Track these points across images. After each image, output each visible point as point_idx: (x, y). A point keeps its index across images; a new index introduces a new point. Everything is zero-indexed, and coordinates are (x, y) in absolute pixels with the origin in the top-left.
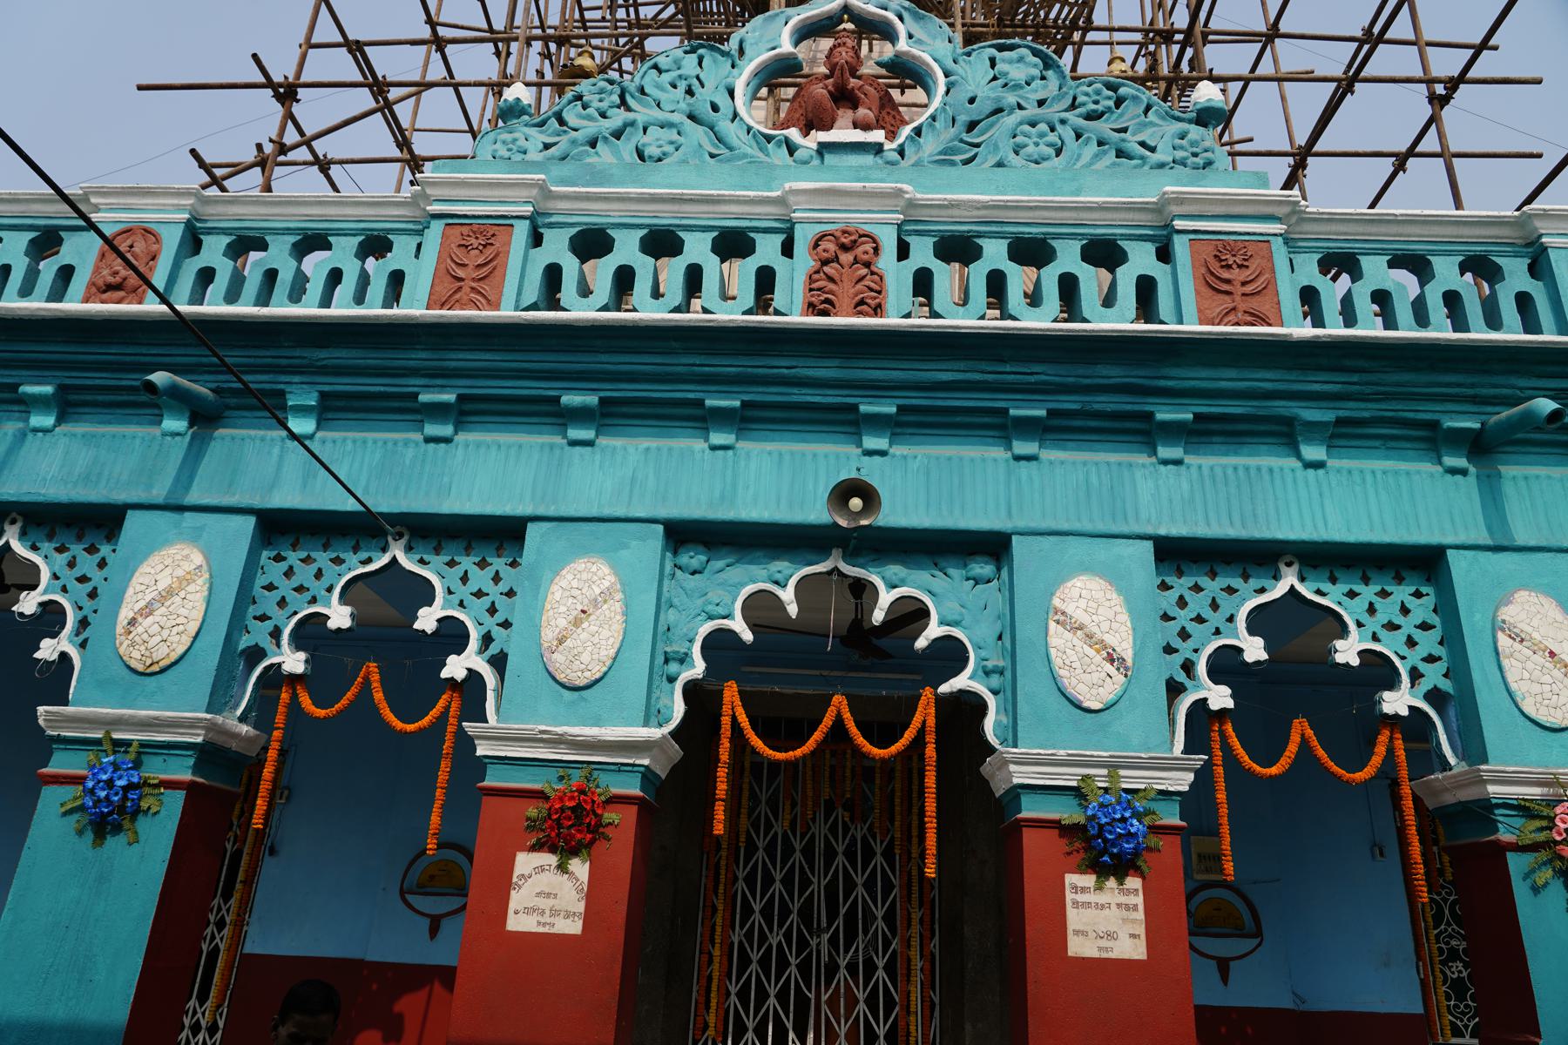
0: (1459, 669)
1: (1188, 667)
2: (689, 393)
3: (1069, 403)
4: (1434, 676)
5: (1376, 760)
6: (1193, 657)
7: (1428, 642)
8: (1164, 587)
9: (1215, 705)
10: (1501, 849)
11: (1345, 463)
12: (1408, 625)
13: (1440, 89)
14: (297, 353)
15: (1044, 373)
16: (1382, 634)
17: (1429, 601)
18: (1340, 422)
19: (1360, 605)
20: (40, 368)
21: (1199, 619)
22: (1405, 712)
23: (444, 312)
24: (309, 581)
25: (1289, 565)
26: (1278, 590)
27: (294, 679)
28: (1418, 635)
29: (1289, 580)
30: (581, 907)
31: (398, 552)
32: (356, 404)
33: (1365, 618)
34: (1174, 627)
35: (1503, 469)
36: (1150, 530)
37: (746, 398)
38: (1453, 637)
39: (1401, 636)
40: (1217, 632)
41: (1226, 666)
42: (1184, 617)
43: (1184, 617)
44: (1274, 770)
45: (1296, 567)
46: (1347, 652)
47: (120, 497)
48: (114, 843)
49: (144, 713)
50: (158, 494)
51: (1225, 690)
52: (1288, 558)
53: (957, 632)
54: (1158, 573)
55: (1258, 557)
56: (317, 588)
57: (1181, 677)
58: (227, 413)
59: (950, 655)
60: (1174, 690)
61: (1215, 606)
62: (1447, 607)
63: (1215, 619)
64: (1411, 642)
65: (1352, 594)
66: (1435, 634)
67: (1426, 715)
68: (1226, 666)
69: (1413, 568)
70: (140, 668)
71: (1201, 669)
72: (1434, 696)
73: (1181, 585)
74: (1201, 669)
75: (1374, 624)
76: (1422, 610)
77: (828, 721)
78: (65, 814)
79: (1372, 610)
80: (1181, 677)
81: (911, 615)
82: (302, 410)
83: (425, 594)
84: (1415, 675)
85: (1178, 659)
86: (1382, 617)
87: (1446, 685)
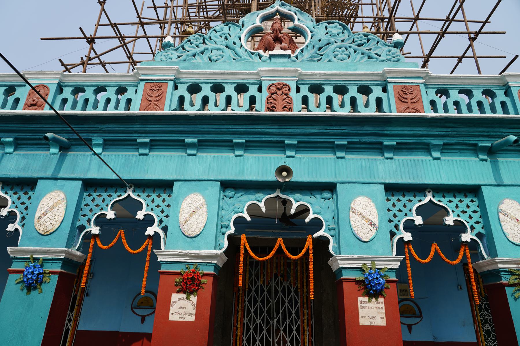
0: (487, 226)
1: (397, 227)
2: (473, 140)
3: (355, 139)
4: (478, 228)
5: (460, 257)
6: (398, 223)
7: (476, 217)
8: (388, 200)
9: (406, 239)
10: (503, 286)
11: (447, 158)
12: (469, 211)
13: (472, 36)
14: (96, 126)
15: (347, 129)
16: (461, 214)
17: (476, 203)
18: (445, 144)
19: (453, 205)
20: (8, 132)
21: (400, 211)
22: (469, 241)
23: (145, 112)
24: (100, 203)
25: (429, 192)
26: (426, 200)
27: (95, 236)
28: (473, 215)
29: (429, 197)
30: (194, 312)
31: (130, 192)
32: (116, 143)
33: (455, 209)
34: (391, 213)
35: (499, 159)
36: (383, 181)
37: (247, 139)
38: (484, 215)
39: (467, 215)
40: (406, 215)
41: (409, 226)
42: (395, 210)
43: (395, 210)
44: (426, 261)
45: (431, 193)
46: (449, 221)
47: (36, 175)
48: (34, 293)
49: (44, 248)
50: (49, 174)
51: (409, 234)
52: (429, 190)
53: (319, 216)
54: (386, 196)
55: (418, 189)
56: (103, 205)
57: (394, 230)
58: (72, 147)
59: (317, 224)
60: (392, 234)
61: (405, 206)
62: (482, 205)
63: (405, 210)
64: (470, 217)
65: (450, 201)
66: (479, 214)
67: (476, 241)
68: (409, 226)
69: (470, 192)
70: (43, 233)
71: (401, 227)
72: (479, 235)
73: (394, 199)
74: (401, 227)
75: (458, 211)
76: (474, 206)
77: (276, 247)
78: (17, 284)
79: (457, 206)
80: (394, 230)
81: (304, 211)
82: (97, 145)
83: (140, 206)
84: (472, 228)
85: (393, 224)
86: (460, 209)
87: (483, 231)
